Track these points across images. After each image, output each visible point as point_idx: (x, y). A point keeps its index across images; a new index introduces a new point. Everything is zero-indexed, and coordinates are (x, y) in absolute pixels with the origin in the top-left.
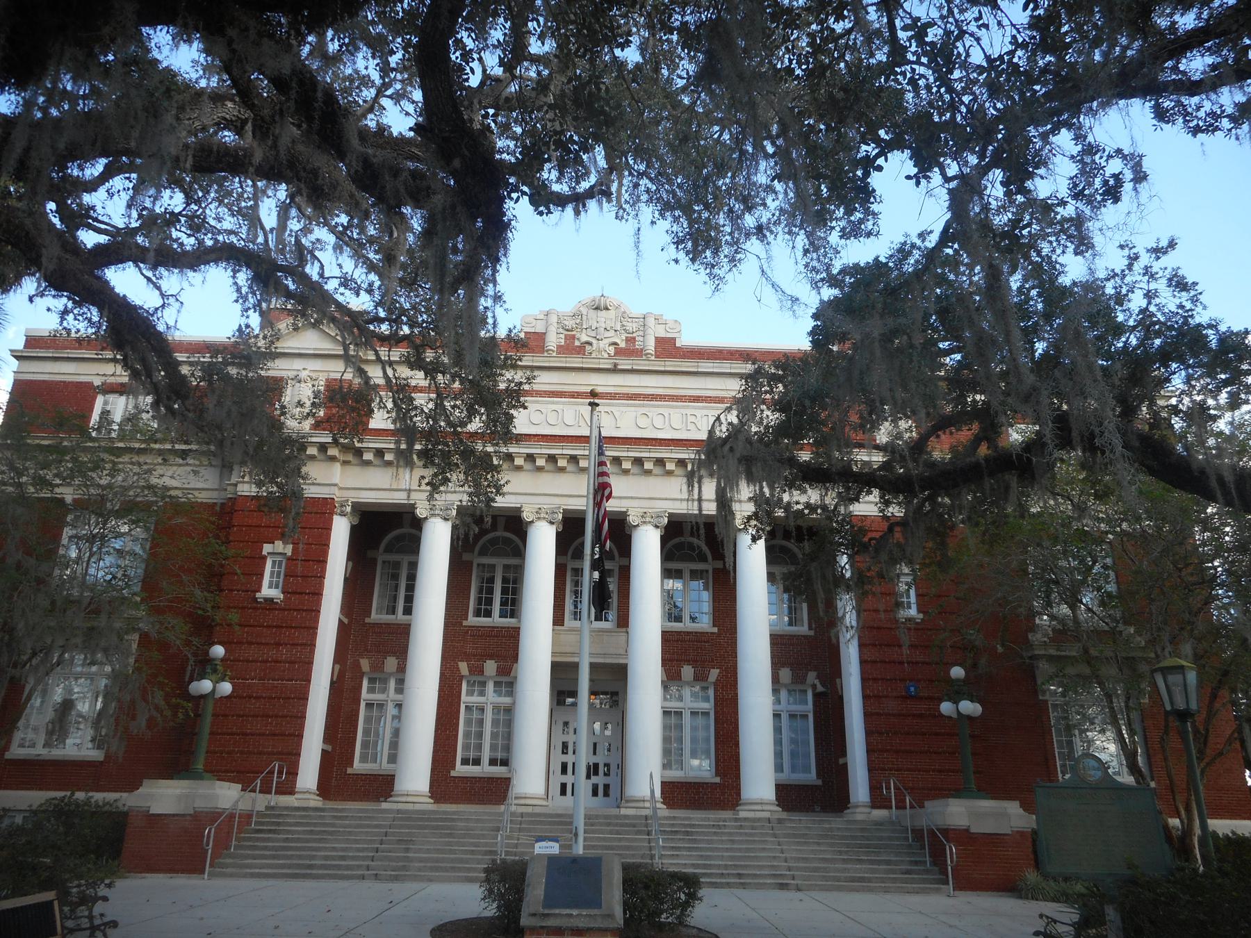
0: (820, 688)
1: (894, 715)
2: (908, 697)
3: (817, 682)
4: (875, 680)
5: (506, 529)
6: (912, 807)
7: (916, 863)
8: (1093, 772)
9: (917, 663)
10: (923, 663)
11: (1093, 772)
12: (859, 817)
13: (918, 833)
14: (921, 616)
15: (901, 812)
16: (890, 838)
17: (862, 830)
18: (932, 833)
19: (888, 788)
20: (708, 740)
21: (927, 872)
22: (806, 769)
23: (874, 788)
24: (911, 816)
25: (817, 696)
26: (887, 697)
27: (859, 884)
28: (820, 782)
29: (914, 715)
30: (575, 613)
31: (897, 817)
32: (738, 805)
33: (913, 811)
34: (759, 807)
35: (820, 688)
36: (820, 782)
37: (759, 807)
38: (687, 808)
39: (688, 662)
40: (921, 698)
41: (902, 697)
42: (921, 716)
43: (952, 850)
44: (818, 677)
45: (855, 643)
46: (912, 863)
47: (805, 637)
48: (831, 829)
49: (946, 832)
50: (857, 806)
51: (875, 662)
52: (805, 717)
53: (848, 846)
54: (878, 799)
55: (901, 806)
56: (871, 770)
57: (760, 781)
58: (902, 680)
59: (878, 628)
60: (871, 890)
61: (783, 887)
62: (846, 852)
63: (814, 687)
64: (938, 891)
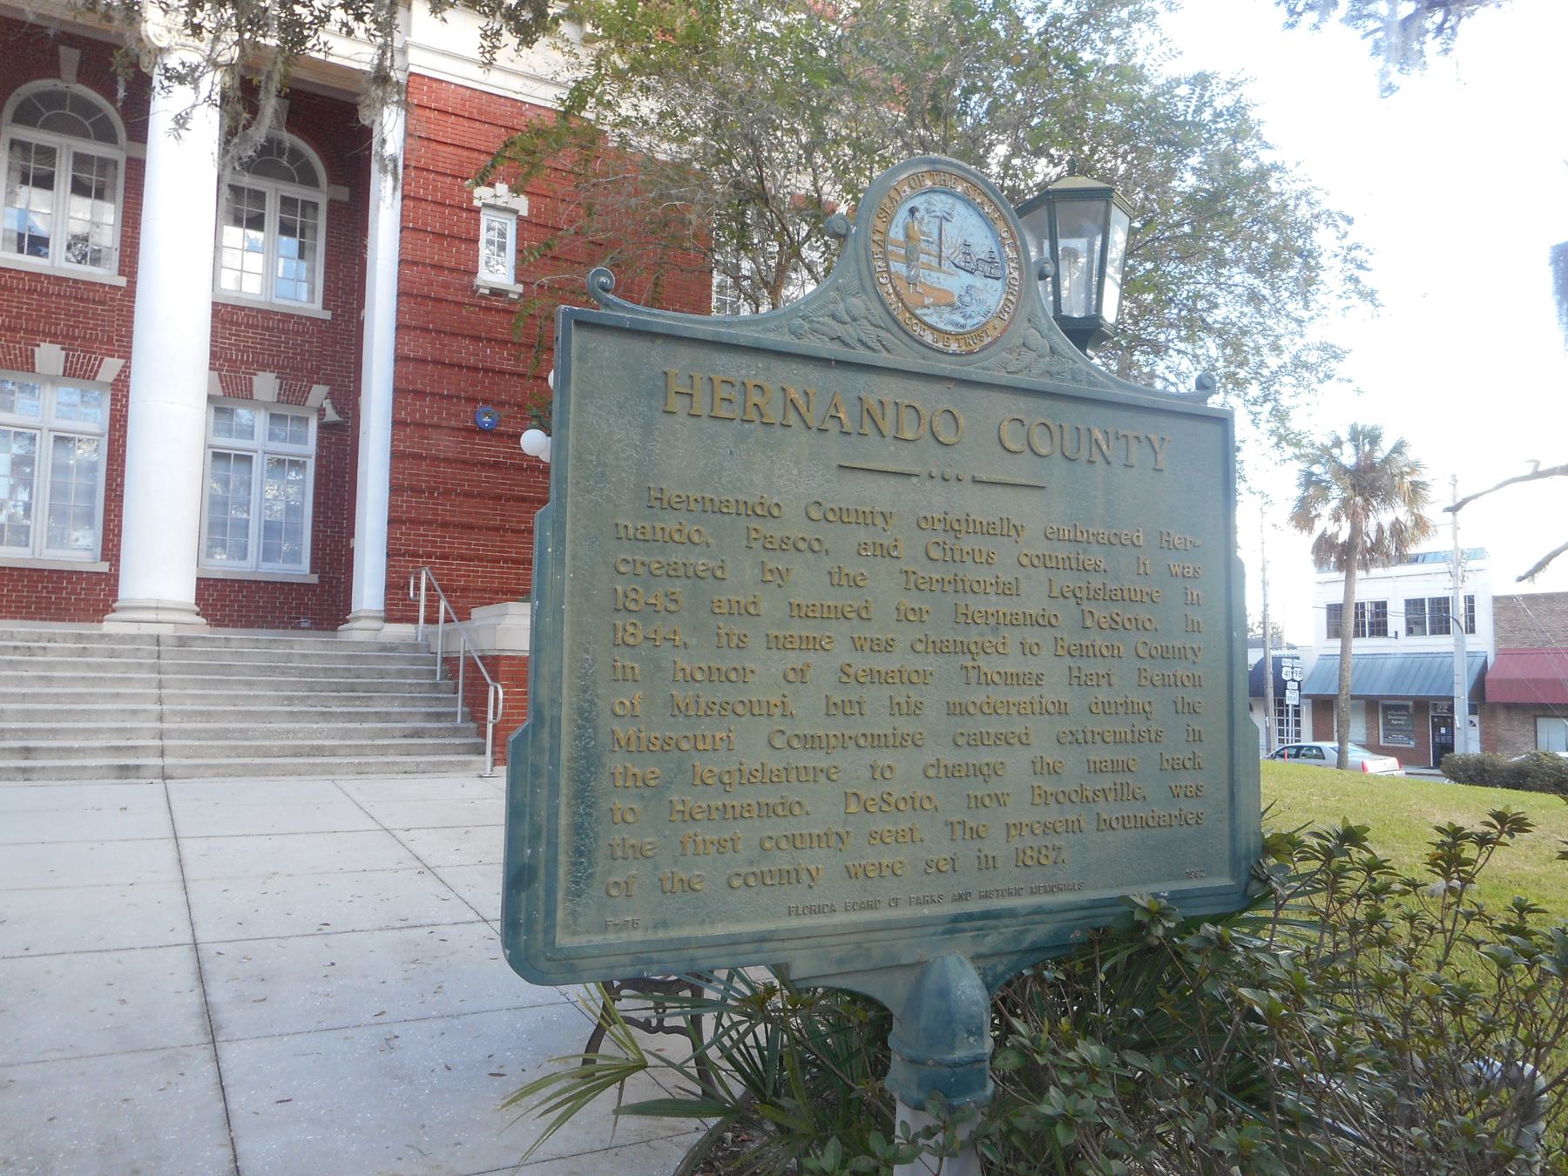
0: (331, 416)
1: (446, 460)
2: (476, 431)
3: (327, 405)
4: (420, 394)
5: (83, 76)
6: (448, 620)
7: (438, 716)
8: (956, 283)
9: (502, 372)
10: (512, 374)
11: (956, 283)
12: (357, 636)
13: (450, 661)
14: (520, 288)
15: (431, 627)
16: (401, 673)
17: (350, 658)
18: (471, 664)
19: (417, 588)
20: (91, 493)
21: (455, 732)
22: (295, 557)
23: (396, 587)
24: (446, 635)
25: (323, 428)
26: (437, 427)
27: (310, 759)
28: (314, 579)
29: (483, 464)
30: (281, 462)
31: (426, 637)
32: (105, 612)
33: (449, 626)
34: (151, 616)
35: (331, 416)
36: (314, 579)
37: (151, 616)
38: (30, 617)
39: (53, 338)
40: (500, 435)
41: (467, 429)
42: (496, 466)
43: (497, 694)
44: (330, 395)
45: (208, 125)
46: (430, 716)
47: (314, 321)
48: (289, 657)
49: (494, 663)
50: (358, 618)
51: (424, 361)
52: (297, 465)
53: (311, 687)
54: (398, 607)
55: (431, 619)
56: (391, 554)
57: (163, 569)
58: (472, 400)
59: (438, 300)
60: (328, 771)
61: (124, 772)
62: (303, 699)
63: (321, 412)
64: (465, 765)
